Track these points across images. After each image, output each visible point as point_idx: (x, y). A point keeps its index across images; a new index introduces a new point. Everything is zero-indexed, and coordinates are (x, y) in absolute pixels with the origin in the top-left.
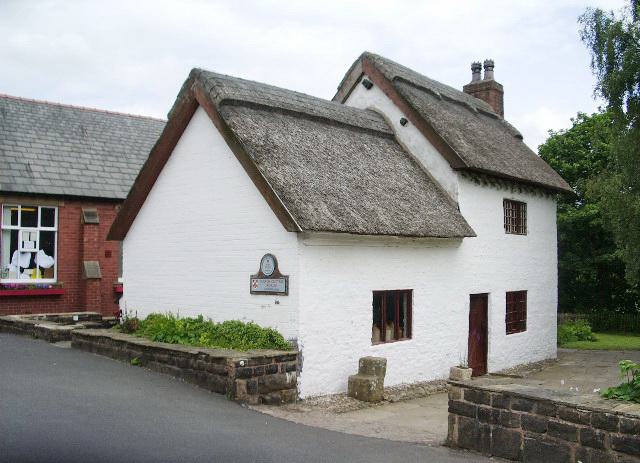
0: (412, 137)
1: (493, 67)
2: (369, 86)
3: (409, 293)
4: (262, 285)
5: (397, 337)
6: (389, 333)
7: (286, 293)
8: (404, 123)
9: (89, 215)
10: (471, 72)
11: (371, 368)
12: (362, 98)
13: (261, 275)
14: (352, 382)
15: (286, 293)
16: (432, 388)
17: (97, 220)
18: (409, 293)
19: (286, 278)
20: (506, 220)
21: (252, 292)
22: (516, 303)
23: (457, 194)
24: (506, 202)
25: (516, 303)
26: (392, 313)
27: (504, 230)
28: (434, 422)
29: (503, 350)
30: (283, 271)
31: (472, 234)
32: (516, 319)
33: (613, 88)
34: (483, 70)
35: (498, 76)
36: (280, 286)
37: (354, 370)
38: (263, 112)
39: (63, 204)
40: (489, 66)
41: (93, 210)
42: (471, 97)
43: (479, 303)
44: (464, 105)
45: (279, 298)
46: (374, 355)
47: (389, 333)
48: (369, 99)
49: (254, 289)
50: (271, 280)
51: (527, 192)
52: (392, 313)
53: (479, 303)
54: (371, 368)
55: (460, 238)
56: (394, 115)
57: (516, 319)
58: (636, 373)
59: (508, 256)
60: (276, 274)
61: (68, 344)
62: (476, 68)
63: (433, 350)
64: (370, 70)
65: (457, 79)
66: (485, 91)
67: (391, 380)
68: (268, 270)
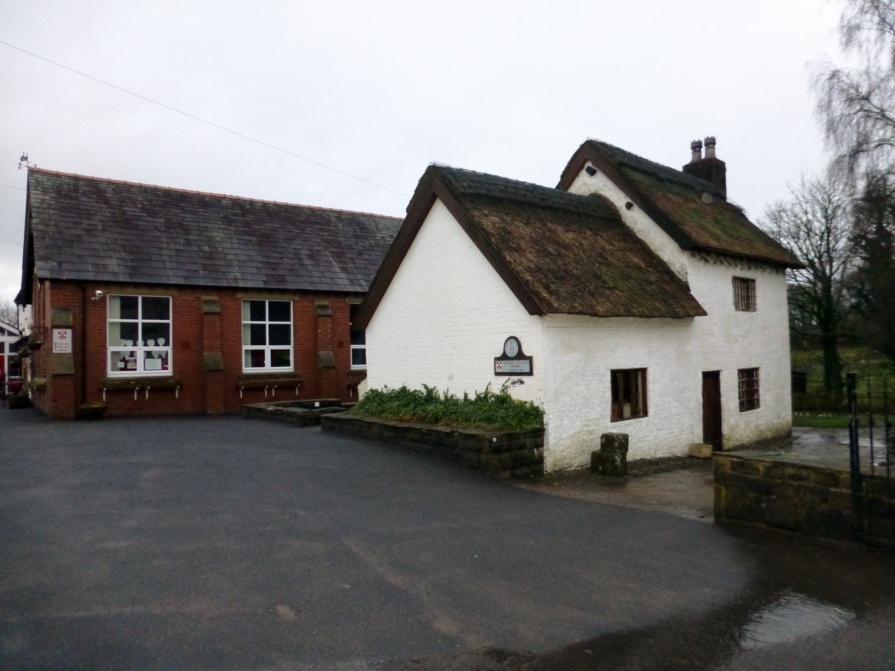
0: (638, 220)
1: (714, 143)
2: (592, 172)
3: (644, 371)
4: (506, 366)
5: (635, 414)
6: (627, 409)
7: (530, 374)
8: (629, 206)
9: (320, 307)
10: (691, 151)
11: (613, 445)
12: (585, 184)
13: (504, 357)
14: (595, 456)
15: (530, 374)
16: (672, 463)
17: (330, 312)
18: (644, 371)
19: (530, 359)
20: (736, 296)
21: (497, 374)
22: (749, 379)
23: (686, 274)
24: (735, 279)
25: (749, 379)
26: (628, 390)
27: (733, 308)
28: (692, 496)
29: (738, 425)
30: (527, 353)
31: (704, 313)
32: (749, 398)
33: (557, 187)
34: (703, 150)
35: (720, 154)
36: (524, 366)
37: (596, 446)
38: (523, 199)
39: (297, 298)
40: (711, 143)
41: (326, 302)
42: (690, 176)
43: (711, 380)
44: (687, 186)
45: (524, 378)
46: (615, 431)
47: (627, 409)
48: (588, 184)
49: (498, 371)
50: (514, 360)
51: (756, 268)
52: (628, 390)
53: (711, 380)
54: (613, 445)
55: (690, 316)
56: (618, 198)
57: (749, 398)
58: (609, 461)
59: (741, 334)
60: (520, 356)
61: (318, 429)
62: (696, 147)
63: (667, 426)
64: (594, 155)
65: (677, 158)
66: (707, 171)
67: (634, 453)
68: (512, 351)
